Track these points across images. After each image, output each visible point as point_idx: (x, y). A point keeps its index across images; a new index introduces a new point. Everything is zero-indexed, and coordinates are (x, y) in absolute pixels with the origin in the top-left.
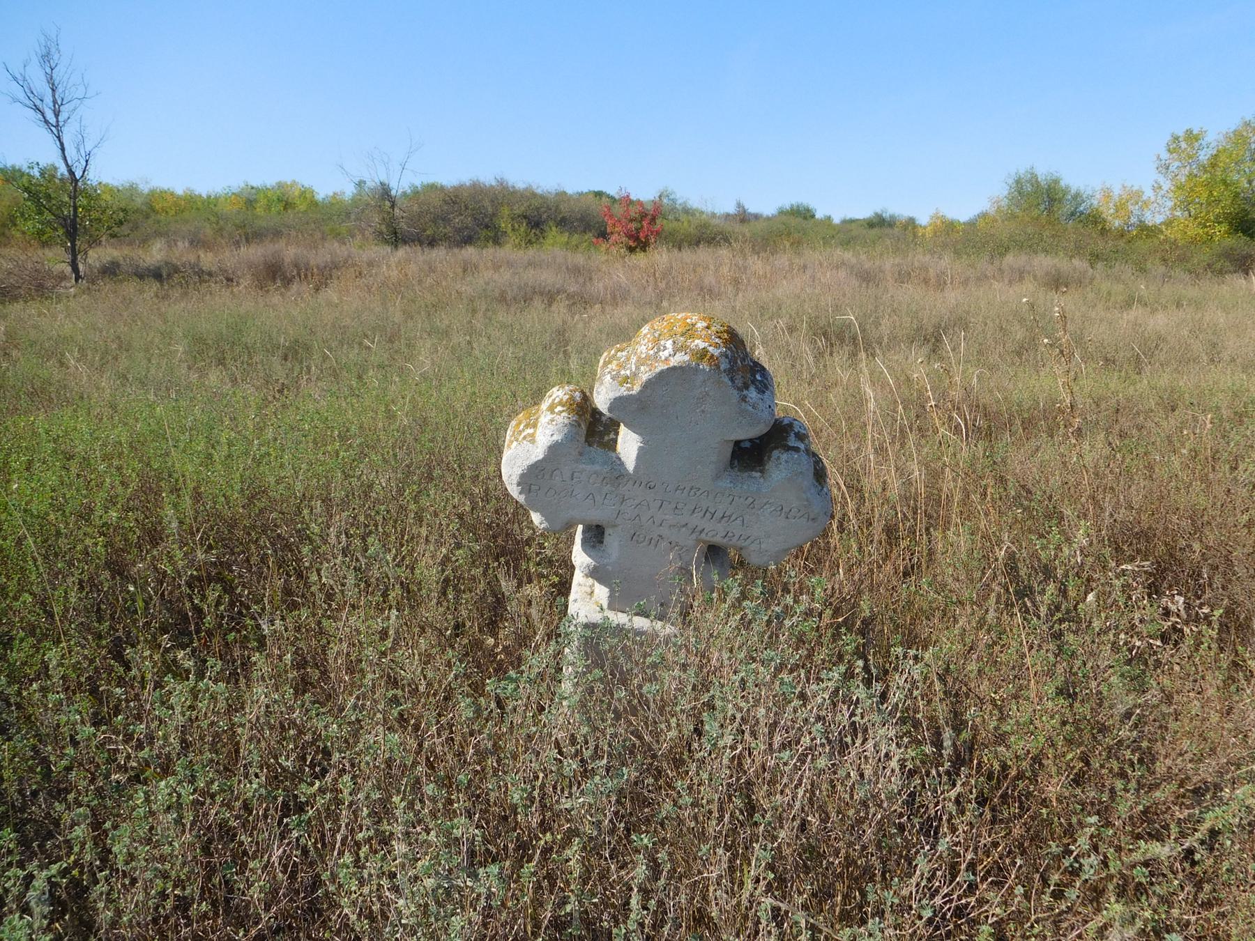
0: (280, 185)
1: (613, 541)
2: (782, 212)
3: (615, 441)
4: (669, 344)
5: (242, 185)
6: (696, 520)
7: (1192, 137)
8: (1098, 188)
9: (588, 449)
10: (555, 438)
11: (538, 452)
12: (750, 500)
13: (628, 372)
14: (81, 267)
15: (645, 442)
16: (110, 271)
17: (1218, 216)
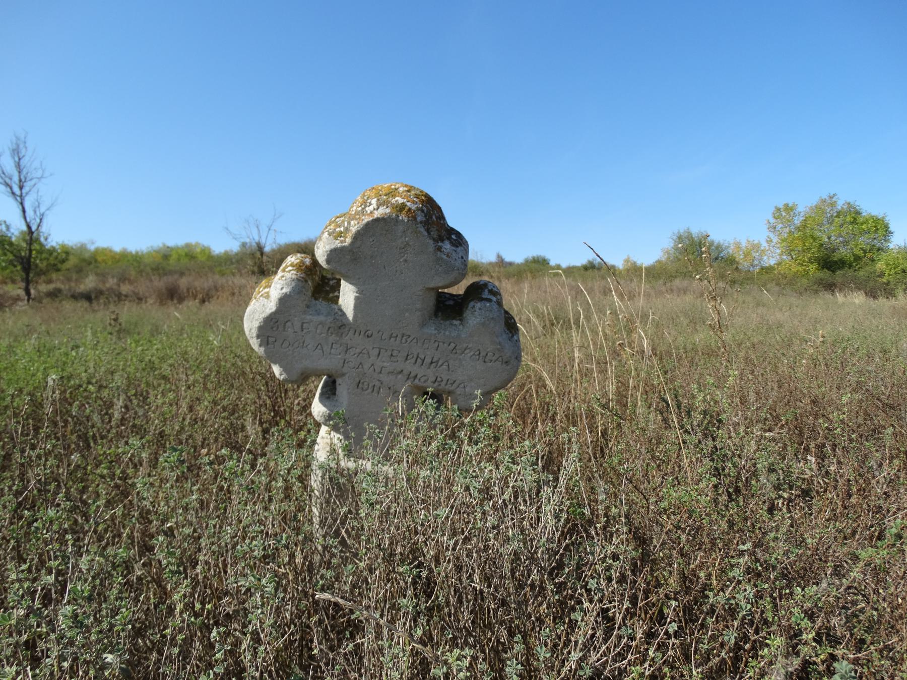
0: (188, 245)
1: (343, 389)
2: (527, 261)
3: (338, 297)
4: (374, 201)
5: (161, 245)
6: (409, 367)
7: (789, 208)
8: (732, 242)
9: (314, 302)
10: (284, 291)
11: (271, 306)
12: (453, 345)
13: (342, 229)
14: (32, 291)
15: (360, 292)
16: (54, 295)
17: (810, 258)
